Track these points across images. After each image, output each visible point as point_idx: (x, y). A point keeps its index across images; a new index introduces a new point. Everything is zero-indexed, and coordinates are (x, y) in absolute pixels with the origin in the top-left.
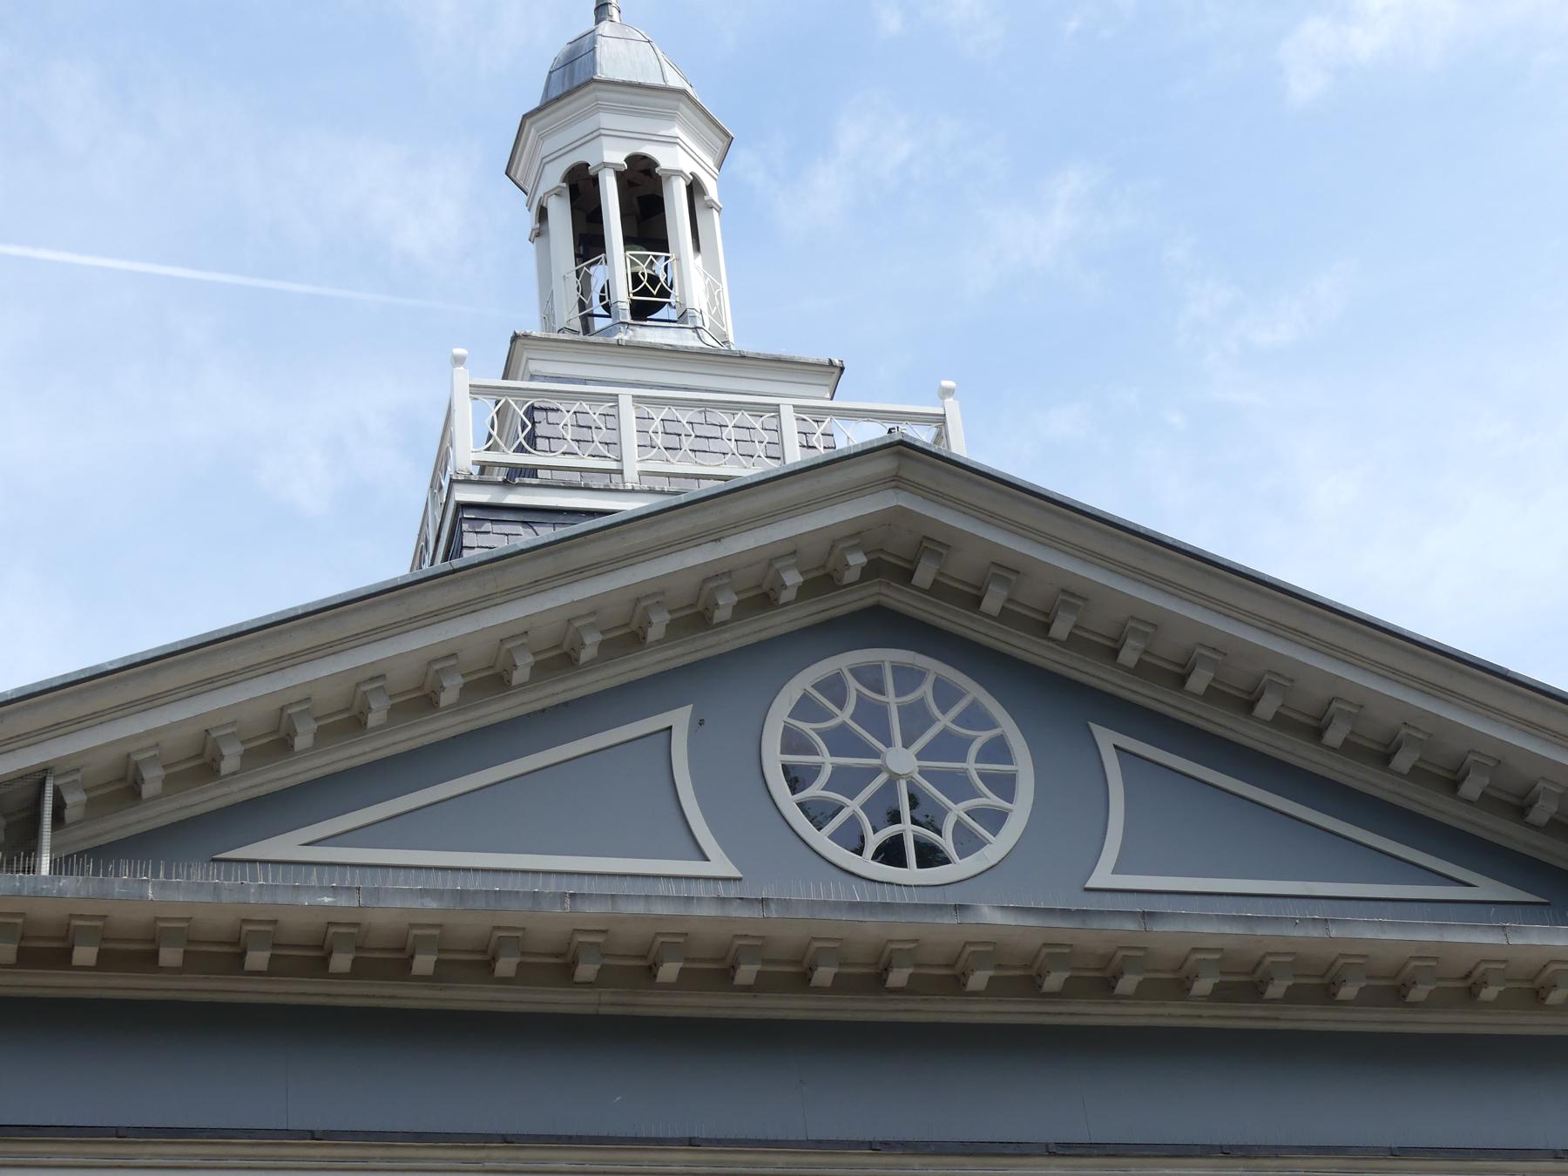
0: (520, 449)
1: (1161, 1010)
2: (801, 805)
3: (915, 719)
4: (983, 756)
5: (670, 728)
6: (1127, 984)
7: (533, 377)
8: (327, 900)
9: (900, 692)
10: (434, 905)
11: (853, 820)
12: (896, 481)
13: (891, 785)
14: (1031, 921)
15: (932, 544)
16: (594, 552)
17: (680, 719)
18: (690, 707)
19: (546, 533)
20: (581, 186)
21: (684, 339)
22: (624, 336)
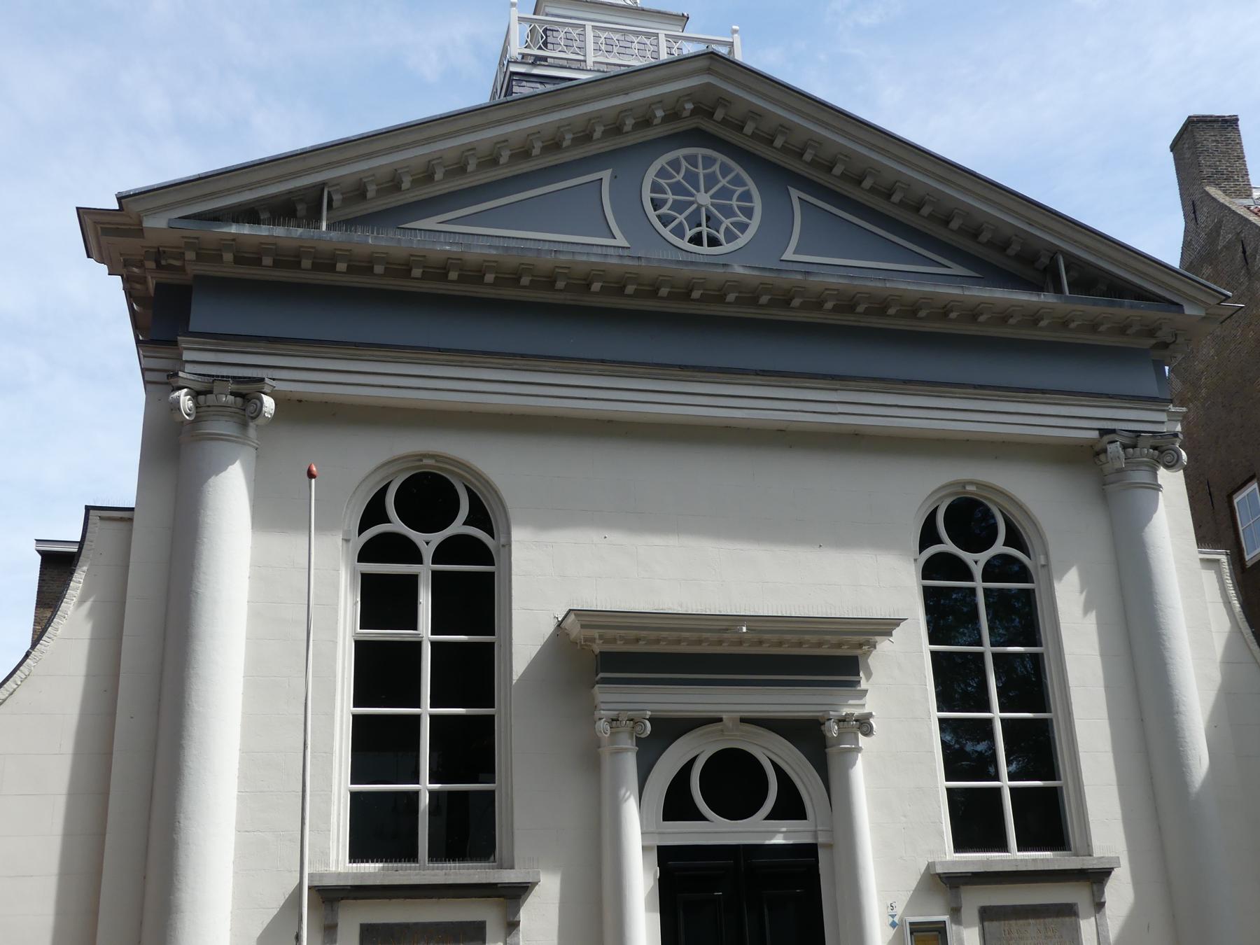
0: (540, 48)
2: (659, 217)
3: (711, 180)
5: (602, 179)
7: (547, 15)
8: (448, 248)
11: (681, 224)
12: (709, 71)
14: (747, 272)
15: (724, 100)
17: (606, 175)
18: (611, 170)
19: (549, 87)
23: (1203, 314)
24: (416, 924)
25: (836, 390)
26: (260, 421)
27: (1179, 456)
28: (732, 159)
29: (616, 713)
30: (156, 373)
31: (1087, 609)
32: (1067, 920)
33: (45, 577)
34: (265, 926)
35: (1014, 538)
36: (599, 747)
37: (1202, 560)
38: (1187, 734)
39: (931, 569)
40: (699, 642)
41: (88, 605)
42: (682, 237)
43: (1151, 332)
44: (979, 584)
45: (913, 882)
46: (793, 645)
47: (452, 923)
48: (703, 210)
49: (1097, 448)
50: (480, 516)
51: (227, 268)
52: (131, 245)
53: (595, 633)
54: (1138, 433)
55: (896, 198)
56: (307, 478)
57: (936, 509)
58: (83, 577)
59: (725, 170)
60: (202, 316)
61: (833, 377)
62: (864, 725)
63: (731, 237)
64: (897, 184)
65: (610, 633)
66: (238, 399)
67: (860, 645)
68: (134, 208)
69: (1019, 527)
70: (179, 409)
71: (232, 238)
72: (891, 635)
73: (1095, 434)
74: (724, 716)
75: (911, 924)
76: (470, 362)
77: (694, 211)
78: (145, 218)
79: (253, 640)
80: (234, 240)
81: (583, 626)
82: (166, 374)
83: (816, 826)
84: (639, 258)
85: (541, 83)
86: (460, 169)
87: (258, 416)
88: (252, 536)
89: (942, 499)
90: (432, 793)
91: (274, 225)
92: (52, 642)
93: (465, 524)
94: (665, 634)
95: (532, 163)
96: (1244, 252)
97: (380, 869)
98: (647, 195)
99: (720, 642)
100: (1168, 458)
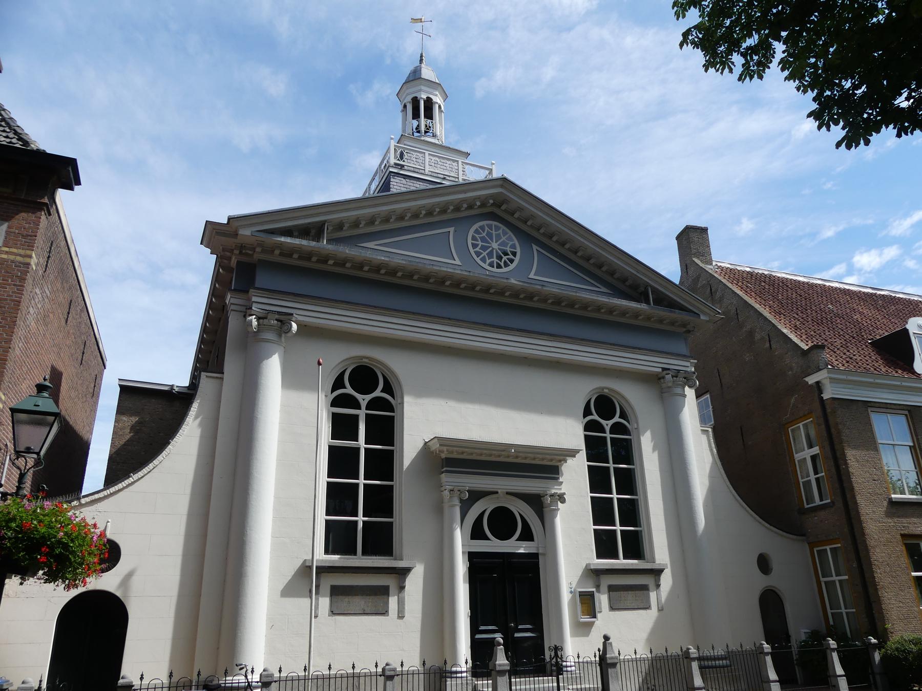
0: (398, 160)
2: (475, 252)
3: (498, 237)
4: (477, 245)
6: (536, 299)
7: (405, 145)
8: (383, 258)
9: (495, 231)
10: (404, 263)
11: (484, 256)
12: (502, 186)
13: (492, 251)
15: (506, 201)
16: (441, 191)
17: (452, 230)
20: (415, 102)
21: (437, 142)
22: (422, 138)
23: (708, 319)
25: (551, 341)
26: (289, 335)
27: (696, 383)
30: (236, 306)
31: (654, 450)
32: (645, 592)
33: (121, 399)
34: (285, 585)
35: (623, 415)
36: (443, 503)
37: (702, 430)
38: (696, 508)
39: (589, 427)
40: (491, 455)
41: (199, 420)
42: (485, 262)
44: (608, 435)
46: (458, 453)
48: (495, 251)
49: (660, 376)
50: (388, 389)
51: (276, 257)
52: (230, 242)
53: (445, 449)
54: (679, 371)
55: (579, 254)
56: (317, 366)
57: (590, 399)
58: (197, 405)
59: (505, 233)
60: (261, 279)
61: (551, 335)
62: (561, 498)
63: (506, 265)
64: (581, 248)
65: (451, 449)
66: (279, 323)
67: (560, 461)
68: (235, 224)
70: (252, 325)
71: (280, 243)
72: (575, 457)
73: (660, 370)
74: (499, 491)
75: (579, 592)
76: (360, 309)
77: (491, 251)
78: (240, 230)
79: (281, 442)
80: (281, 244)
81: (440, 445)
82: (246, 307)
83: (538, 545)
84: (470, 271)
85: (404, 178)
86: (387, 220)
88: (282, 392)
89: (594, 394)
90: (364, 522)
91: (302, 239)
92: (181, 437)
93: (381, 392)
94: (476, 451)
95: (419, 221)
96: (711, 290)
97: (340, 558)
98: (470, 241)
99: (517, 457)
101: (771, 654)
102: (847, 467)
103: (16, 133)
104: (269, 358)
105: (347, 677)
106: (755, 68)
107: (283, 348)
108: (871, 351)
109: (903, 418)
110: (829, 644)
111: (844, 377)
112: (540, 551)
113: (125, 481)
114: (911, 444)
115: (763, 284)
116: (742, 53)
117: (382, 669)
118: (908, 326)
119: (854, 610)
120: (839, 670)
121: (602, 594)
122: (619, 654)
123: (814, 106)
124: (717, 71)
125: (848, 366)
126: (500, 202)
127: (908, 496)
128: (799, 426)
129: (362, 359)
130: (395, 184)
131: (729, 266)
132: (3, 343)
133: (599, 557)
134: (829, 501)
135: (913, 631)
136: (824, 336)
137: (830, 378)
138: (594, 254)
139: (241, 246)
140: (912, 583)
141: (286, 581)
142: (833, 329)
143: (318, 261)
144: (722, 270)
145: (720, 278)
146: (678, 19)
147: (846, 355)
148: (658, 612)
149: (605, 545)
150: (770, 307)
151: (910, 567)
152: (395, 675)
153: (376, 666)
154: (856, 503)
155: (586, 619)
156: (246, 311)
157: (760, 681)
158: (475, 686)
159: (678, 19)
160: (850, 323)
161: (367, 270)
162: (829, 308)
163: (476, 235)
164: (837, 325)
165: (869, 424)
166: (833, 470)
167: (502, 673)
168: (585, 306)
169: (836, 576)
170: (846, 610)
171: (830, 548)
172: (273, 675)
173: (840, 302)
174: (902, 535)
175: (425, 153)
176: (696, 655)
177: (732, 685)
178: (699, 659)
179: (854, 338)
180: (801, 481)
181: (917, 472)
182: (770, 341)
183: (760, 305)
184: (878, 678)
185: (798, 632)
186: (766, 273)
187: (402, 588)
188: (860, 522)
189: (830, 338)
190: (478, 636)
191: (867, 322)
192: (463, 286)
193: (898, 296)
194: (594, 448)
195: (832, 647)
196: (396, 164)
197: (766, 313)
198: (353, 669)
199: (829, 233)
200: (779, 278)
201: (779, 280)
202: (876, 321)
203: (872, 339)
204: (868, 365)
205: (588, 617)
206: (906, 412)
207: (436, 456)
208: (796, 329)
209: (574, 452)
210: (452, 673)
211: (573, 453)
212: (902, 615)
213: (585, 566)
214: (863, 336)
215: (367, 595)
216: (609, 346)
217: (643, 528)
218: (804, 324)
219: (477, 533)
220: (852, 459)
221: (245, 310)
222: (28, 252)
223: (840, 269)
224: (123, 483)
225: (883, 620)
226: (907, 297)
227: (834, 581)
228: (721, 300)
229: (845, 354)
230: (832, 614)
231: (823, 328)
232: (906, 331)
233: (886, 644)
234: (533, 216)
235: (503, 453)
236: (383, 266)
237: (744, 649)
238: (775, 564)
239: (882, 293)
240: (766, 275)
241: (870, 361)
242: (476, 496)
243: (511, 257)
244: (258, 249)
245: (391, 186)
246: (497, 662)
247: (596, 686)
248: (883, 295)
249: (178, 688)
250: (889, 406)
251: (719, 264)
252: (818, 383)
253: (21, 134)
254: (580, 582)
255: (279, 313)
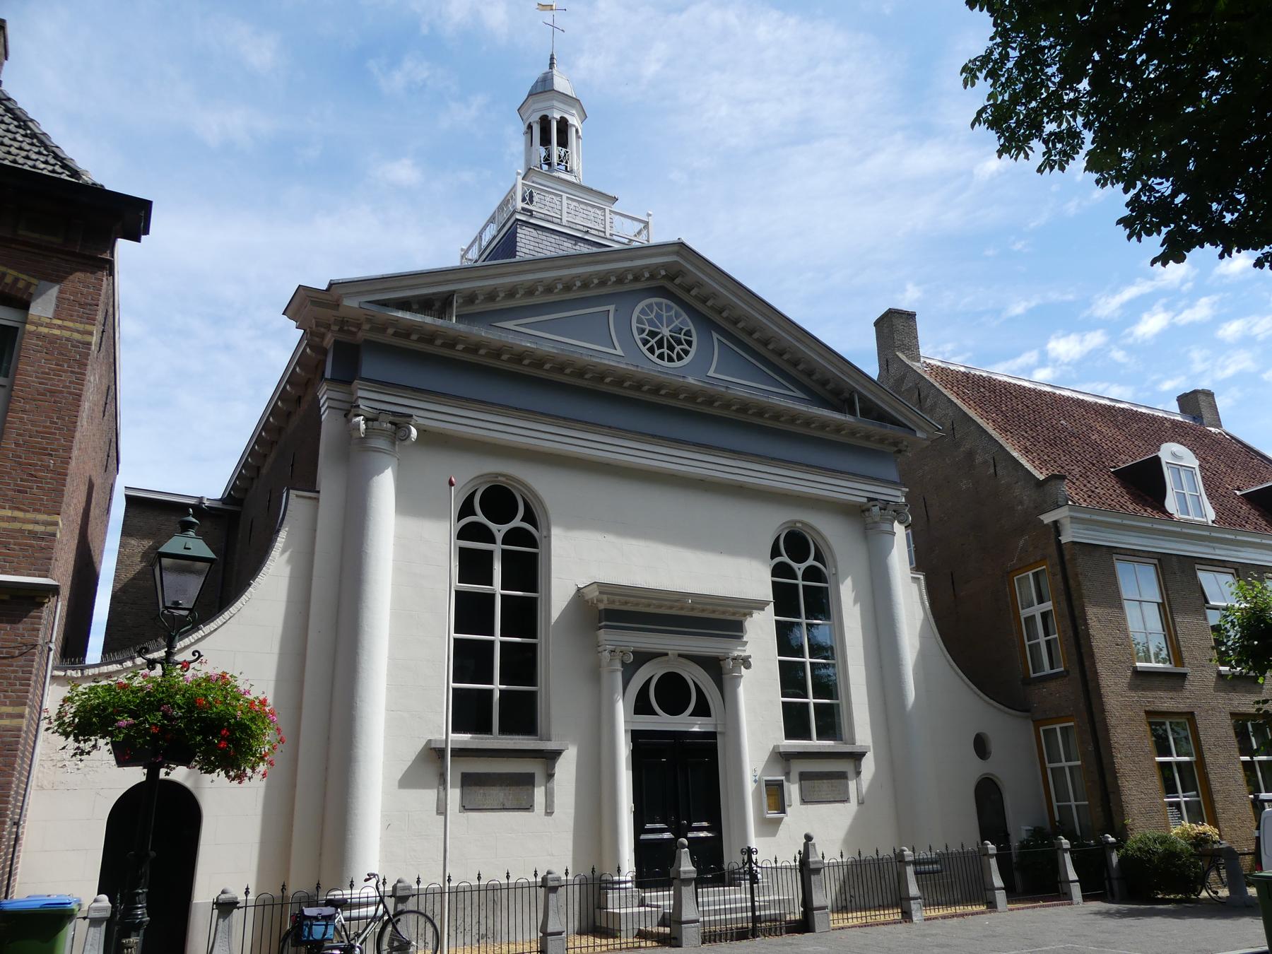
0: (527, 203)
1: (723, 412)
7: (533, 182)
8: (529, 345)
10: (556, 351)
11: (652, 346)
12: (678, 253)
13: (662, 339)
14: (700, 384)
17: (612, 308)
19: (595, 250)
20: (545, 122)
24: (494, 774)
26: (407, 443)
28: (682, 309)
29: (614, 647)
30: (336, 402)
31: (855, 602)
32: (843, 781)
34: (403, 772)
35: (819, 557)
37: (912, 577)
39: (778, 570)
41: (287, 555)
43: (895, 444)
44: (800, 583)
45: (766, 756)
47: (521, 774)
49: (864, 508)
50: (530, 517)
51: (388, 338)
52: (328, 314)
53: (605, 597)
60: (369, 367)
63: (680, 358)
66: (394, 427)
67: (745, 615)
69: (532, 507)
73: (865, 500)
74: (670, 652)
78: (344, 299)
80: (397, 321)
81: (600, 593)
83: (716, 721)
84: (637, 366)
87: (405, 439)
89: (783, 530)
90: (501, 691)
93: (521, 520)
94: (632, 599)
96: (919, 395)
97: (471, 738)
99: (714, 612)
100: (902, 518)
101: (996, 855)
102: (1087, 629)
103: (56, 157)
104: (380, 474)
105: (529, 887)
106: (1058, 157)
107: (396, 459)
108: (1115, 482)
109: (1152, 568)
110: (1061, 843)
111: (1087, 516)
112: (719, 730)
113: (193, 635)
114: (1160, 601)
115: (982, 390)
116: (1044, 139)
117: (393, 887)
118: (1160, 454)
119: (1087, 803)
120: (1072, 875)
121: (793, 784)
122: (823, 857)
123: (1127, 212)
124: (1011, 157)
125: (1091, 501)
126: (673, 274)
127: (1154, 665)
128: (1028, 575)
129: (497, 477)
130: (523, 236)
131: (940, 364)
132: (61, 451)
133: (456, 729)
134: (1062, 669)
135: (1156, 828)
136: (1060, 462)
137: (1071, 517)
138: (789, 347)
139: (342, 321)
140: (1156, 771)
141: (405, 768)
142: (1070, 452)
143: (444, 345)
144: (932, 370)
145: (932, 380)
146: (965, 88)
147: (1087, 488)
148: (858, 806)
149: (795, 723)
150: (994, 421)
151: (1155, 751)
152: (559, 886)
153: (536, 875)
154: (1096, 673)
155: (772, 815)
156: (349, 410)
157: (983, 888)
158: (642, 899)
159: (965, 88)
160: (1087, 445)
161: (461, 349)
162: (1062, 425)
163: (642, 317)
164: (1073, 448)
165: (1113, 574)
166: (1070, 633)
167: (687, 882)
168: (777, 415)
169: (1066, 761)
170: (1076, 803)
171: (1061, 728)
172: (411, 887)
173: (1074, 417)
174: (1147, 712)
175: (561, 196)
176: (911, 859)
177: (943, 895)
178: (916, 863)
179: (1094, 465)
180: (1027, 643)
181: (1165, 635)
182: (995, 466)
183: (982, 419)
184: (1115, 883)
185: (1019, 830)
186: (984, 374)
187: (550, 776)
188: (1100, 696)
189: (1067, 465)
190: (643, 837)
191: (1107, 444)
192: (627, 384)
193: (1140, 410)
194: (784, 599)
195: (1065, 846)
196: (523, 209)
197: (989, 428)
198: (508, 879)
199: (1018, 309)
200: (1000, 381)
201: (1000, 385)
202: (1117, 444)
203: (1114, 467)
204: (1112, 500)
205: (776, 812)
206: (1156, 561)
207: (591, 606)
208: (1026, 451)
209: (762, 604)
210: (614, 883)
211: (760, 605)
212: (1144, 808)
213: (772, 748)
214: (1104, 463)
215: (507, 786)
216: (804, 468)
217: (841, 701)
218: (1035, 446)
219: (642, 706)
220: (1093, 618)
221: (349, 408)
222: (89, 327)
223: (1030, 357)
224: (191, 637)
225: (1122, 815)
226: (1151, 412)
227: (1063, 768)
228: (931, 410)
229: (1085, 486)
230: (1058, 807)
231: (1058, 450)
232: (1157, 461)
233: (1125, 843)
234: (716, 295)
235: (676, 604)
236: (528, 354)
237: (950, 851)
238: (995, 747)
239: (1122, 406)
240: (984, 378)
241: (1115, 496)
242: (642, 658)
243: (686, 347)
244: (366, 327)
245: (518, 239)
246: (681, 869)
247: (781, 897)
248: (1123, 409)
249: (266, 907)
250: (1137, 553)
251: (928, 361)
252: (1056, 523)
253: (64, 159)
254: (767, 768)
255: (394, 413)
